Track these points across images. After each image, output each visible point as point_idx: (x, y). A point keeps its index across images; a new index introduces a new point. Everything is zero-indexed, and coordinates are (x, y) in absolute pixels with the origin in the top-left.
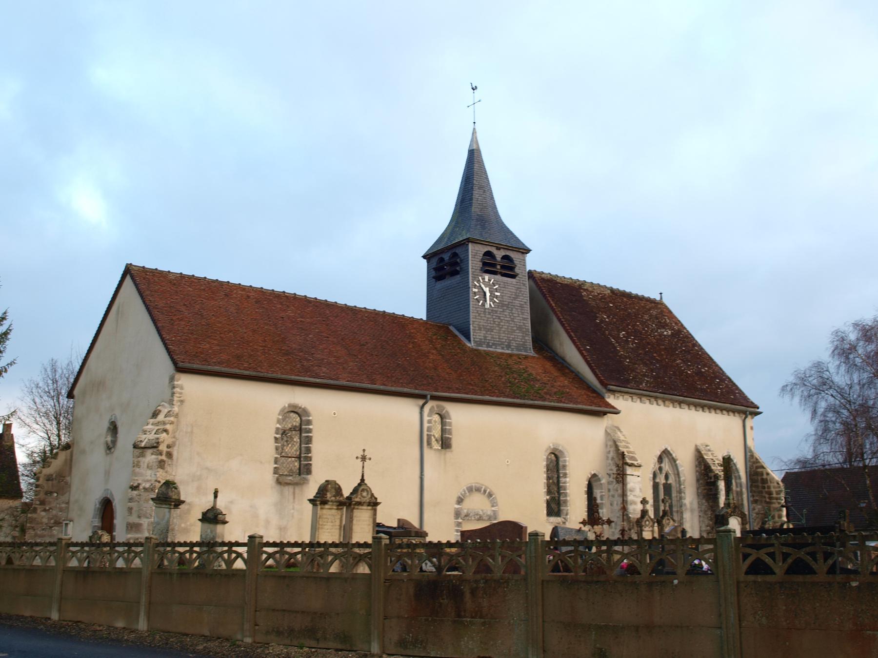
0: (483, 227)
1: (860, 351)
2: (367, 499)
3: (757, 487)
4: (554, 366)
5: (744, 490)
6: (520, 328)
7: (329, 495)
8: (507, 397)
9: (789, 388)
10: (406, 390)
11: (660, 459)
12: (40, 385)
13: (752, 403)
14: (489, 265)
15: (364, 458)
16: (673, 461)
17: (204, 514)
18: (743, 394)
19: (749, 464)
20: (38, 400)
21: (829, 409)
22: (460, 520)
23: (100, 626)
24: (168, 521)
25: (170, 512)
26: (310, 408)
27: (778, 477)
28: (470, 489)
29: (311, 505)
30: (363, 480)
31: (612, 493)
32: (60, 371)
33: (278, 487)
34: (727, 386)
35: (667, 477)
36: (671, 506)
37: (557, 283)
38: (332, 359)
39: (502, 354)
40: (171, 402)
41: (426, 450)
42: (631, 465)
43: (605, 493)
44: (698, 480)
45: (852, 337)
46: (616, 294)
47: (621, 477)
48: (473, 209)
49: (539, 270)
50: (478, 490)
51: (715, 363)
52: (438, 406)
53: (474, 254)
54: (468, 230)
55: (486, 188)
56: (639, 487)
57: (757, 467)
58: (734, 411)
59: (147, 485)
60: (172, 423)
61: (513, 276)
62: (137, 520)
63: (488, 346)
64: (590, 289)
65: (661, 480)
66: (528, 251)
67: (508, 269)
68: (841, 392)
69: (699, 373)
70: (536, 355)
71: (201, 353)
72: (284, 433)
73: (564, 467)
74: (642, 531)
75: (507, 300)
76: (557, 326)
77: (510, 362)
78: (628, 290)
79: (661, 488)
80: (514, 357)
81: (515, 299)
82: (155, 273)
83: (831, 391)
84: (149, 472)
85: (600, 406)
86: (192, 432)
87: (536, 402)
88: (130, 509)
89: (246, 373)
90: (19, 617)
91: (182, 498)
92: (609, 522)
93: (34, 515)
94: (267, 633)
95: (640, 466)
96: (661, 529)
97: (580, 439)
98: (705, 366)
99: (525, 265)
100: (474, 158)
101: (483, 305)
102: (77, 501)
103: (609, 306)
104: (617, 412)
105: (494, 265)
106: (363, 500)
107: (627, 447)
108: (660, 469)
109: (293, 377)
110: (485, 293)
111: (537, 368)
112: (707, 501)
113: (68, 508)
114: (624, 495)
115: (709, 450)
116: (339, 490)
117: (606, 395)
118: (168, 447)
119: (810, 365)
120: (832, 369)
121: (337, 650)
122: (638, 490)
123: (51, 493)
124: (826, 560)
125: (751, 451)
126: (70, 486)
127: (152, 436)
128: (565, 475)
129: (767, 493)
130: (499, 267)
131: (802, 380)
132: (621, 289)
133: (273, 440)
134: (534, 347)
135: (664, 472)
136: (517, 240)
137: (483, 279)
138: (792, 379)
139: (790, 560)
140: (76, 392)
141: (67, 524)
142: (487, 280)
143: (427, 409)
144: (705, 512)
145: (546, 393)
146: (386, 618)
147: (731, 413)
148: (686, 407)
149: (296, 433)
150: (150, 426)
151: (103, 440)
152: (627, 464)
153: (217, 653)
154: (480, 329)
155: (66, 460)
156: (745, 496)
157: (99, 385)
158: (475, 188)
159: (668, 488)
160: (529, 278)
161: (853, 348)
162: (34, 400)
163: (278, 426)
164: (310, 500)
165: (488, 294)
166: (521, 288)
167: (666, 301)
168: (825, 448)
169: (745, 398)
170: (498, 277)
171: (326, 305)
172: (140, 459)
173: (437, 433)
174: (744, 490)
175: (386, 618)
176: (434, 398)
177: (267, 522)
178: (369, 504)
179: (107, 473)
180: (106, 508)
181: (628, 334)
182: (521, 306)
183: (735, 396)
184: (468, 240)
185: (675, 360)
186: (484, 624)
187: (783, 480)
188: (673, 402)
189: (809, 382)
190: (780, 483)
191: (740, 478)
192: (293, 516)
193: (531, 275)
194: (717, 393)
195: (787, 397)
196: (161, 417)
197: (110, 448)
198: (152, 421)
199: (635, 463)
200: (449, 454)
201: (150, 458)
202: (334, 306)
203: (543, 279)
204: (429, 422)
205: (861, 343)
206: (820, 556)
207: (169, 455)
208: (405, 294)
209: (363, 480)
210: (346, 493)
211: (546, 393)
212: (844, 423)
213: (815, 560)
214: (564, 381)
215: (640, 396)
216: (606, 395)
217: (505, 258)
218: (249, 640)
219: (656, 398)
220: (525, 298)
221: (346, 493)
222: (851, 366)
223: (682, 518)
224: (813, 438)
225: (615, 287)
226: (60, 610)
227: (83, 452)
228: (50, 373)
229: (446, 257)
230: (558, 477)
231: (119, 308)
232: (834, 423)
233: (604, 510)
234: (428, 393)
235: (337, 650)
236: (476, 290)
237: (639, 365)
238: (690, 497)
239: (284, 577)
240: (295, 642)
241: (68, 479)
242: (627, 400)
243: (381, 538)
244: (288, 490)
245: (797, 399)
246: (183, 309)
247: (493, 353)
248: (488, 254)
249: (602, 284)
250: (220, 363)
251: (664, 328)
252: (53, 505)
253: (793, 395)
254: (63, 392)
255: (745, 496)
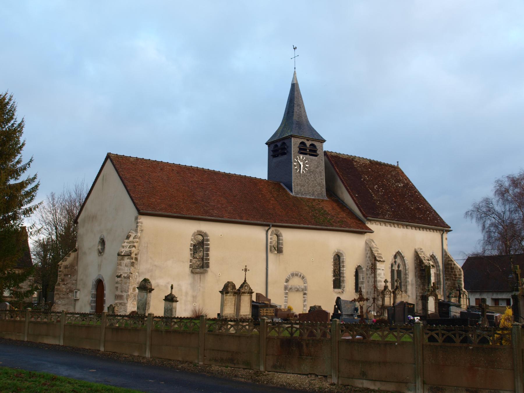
0: (300, 128)
1: (511, 192)
2: (247, 290)
3: (448, 271)
4: (338, 205)
5: (441, 273)
6: (319, 184)
7: (229, 289)
8: (313, 225)
9: (470, 213)
10: (259, 222)
11: (395, 257)
12: (46, 207)
13: (447, 225)
14: (303, 150)
15: (246, 270)
16: (402, 258)
17: (166, 297)
18: (442, 219)
19: (444, 259)
20: (44, 215)
21: (492, 225)
22: (287, 291)
23: (126, 354)
24: (146, 299)
25: (147, 295)
26: (208, 233)
27: (459, 264)
28: (293, 275)
29: (220, 294)
30: (245, 281)
31: (369, 275)
32: (56, 199)
33: (192, 275)
34: (433, 215)
35: (399, 266)
36: (400, 283)
37: (340, 158)
38: (219, 205)
39: (310, 199)
40: (136, 231)
41: (270, 255)
42: (379, 261)
43: (365, 276)
44: (416, 268)
45: (507, 184)
46: (373, 163)
47: (374, 269)
48: (294, 118)
49: (330, 151)
50: (297, 275)
51: (427, 202)
52: (276, 230)
53: (295, 143)
54: (291, 131)
55: (301, 105)
56: (384, 273)
57: (449, 261)
58: (436, 230)
59: (126, 275)
60: (137, 242)
61: (316, 156)
62: (120, 294)
63: (302, 194)
64: (358, 161)
65: (396, 268)
66: (324, 141)
67: (313, 151)
68: (499, 215)
69: (418, 209)
70: (328, 199)
71: (151, 204)
72: (194, 246)
73: (343, 262)
74: (384, 297)
75: (312, 168)
76: (340, 183)
77: (314, 203)
78: (379, 161)
79: (395, 272)
80: (317, 201)
81: (317, 168)
82: (123, 157)
83: (493, 215)
84: (126, 268)
85: (363, 229)
86: (147, 246)
87: (328, 227)
88: (117, 288)
89: (176, 215)
90: (84, 350)
91: (153, 288)
92: (367, 300)
93: (59, 287)
94: (210, 360)
95: (384, 261)
96: (395, 298)
97: (351, 246)
98: (421, 204)
99: (322, 149)
100: (294, 88)
101: (300, 172)
102: (82, 280)
103: (368, 171)
104: (372, 232)
105: (305, 150)
106: (246, 291)
107: (377, 251)
108: (395, 262)
109: (200, 217)
110: (300, 165)
111: (329, 207)
112: (420, 280)
113: (76, 283)
114: (375, 277)
115: (422, 252)
116: (234, 286)
117: (366, 222)
118: (136, 255)
119: (481, 200)
120: (494, 201)
121: (244, 369)
122: (383, 274)
123: (67, 275)
124: (459, 337)
125: (445, 252)
126: (77, 272)
127: (127, 249)
128: (343, 266)
129: (453, 275)
130: (308, 150)
131: (478, 209)
132: (375, 160)
133: (189, 250)
134: (327, 194)
135: (397, 264)
136: (319, 135)
137: (300, 157)
138: (471, 208)
139: (445, 337)
140: (79, 220)
141: (76, 292)
142: (301, 158)
143: (270, 232)
144: (419, 286)
145: (333, 222)
146: (267, 355)
147: (435, 231)
148: (410, 228)
149: (200, 247)
150: (126, 244)
151: (96, 248)
152: (377, 260)
153: (189, 370)
154: (297, 185)
155: (75, 257)
156: (442, 276)
157: (93, 218)
158: (295, 106)
159: (399, 272)
160: (325, 155)
161: (507, 191)
162: (42, 215)
163: (192, 242)
164: (220, 292)
165: (302, 166)
166: (320, 161)
167: (400, 166)
168: (490, 247)
169: (443, 222)
170: (308, 156)
171: (214, 173)
172: (122, 261)
173: (275, 243)
174: (441, 273)
175: (267, 355)
176: (273, 226)
177: (187, 293)
178: (248, 293)
179: (100, 266)
180: (99, 285)
181: (379, 187)
182: (320, 172)
183: (437, 221)
184: (292, 136)
185: (405, 201)
186: (312, 359)
187: (462, 268)
188: (403, 225)
189: (481, 210)
190: (461, 269)
191: (439, 266)
192: (200, 290)
193: (326, 153)
194: (427, 220)
195: (469, 219)
196: (131, 239)
197: (101, 252)
198: (126, 241)
199: (381, 260)
200: (281, 256)
201: (127, 261)
202: (218, 173)
203: (332, 156)
204: (271, 239)
205: (512, 188)
206: (457, 335)
207: (136, 259)
208: (257, 167)
209: (245, 281)
210: (237, 287)
211: (333, 222)
212: (500, 233)
213: (455, 336)
214: (343, 215)
215: (385, 223)
216: (366, 222)
217: (311, 146)
218: (201, 363)
219: (394, 224)
220: (322, 168)
221: (237, 287)
222: (505, 201)
223: (406, 289)
224: (482, 242)
225: (372, 159)
226: (104, 346)
227: (85, 253)
228: (51, 200)
229: (279, 144)
230: (340, 267)
231: (103, 176)
232: (494, 233)
233: (364, 285)
234: (271, 224)
235: (244, 369)
236: (296, 164)
237: (384, 205)
238: (411, 277)
239: (218, 335)
240: (224, 365)
241: (76, 267)
242: (377, 225)
243: (264, 319)
244: (197, 276)
245: (474, 220)
246: (139, 178)
247: (305, 198)
248: (302, 143)
249: (364, 157)
250: (161, 210)
251: (399, 182)
252: (68, 281)
253: (472, 217)
254: (58, 211)
255: (442, 276)
